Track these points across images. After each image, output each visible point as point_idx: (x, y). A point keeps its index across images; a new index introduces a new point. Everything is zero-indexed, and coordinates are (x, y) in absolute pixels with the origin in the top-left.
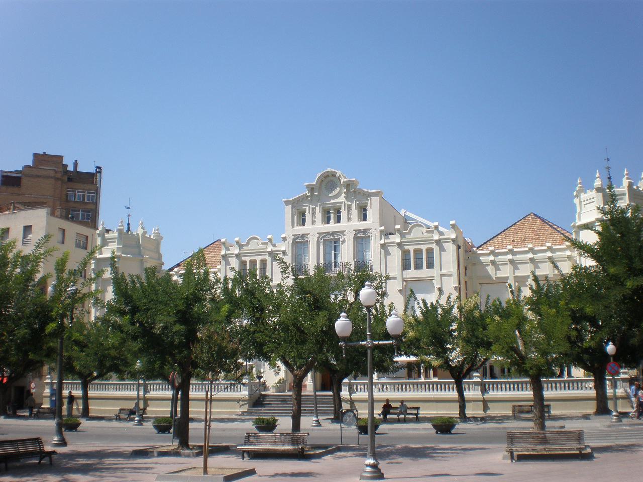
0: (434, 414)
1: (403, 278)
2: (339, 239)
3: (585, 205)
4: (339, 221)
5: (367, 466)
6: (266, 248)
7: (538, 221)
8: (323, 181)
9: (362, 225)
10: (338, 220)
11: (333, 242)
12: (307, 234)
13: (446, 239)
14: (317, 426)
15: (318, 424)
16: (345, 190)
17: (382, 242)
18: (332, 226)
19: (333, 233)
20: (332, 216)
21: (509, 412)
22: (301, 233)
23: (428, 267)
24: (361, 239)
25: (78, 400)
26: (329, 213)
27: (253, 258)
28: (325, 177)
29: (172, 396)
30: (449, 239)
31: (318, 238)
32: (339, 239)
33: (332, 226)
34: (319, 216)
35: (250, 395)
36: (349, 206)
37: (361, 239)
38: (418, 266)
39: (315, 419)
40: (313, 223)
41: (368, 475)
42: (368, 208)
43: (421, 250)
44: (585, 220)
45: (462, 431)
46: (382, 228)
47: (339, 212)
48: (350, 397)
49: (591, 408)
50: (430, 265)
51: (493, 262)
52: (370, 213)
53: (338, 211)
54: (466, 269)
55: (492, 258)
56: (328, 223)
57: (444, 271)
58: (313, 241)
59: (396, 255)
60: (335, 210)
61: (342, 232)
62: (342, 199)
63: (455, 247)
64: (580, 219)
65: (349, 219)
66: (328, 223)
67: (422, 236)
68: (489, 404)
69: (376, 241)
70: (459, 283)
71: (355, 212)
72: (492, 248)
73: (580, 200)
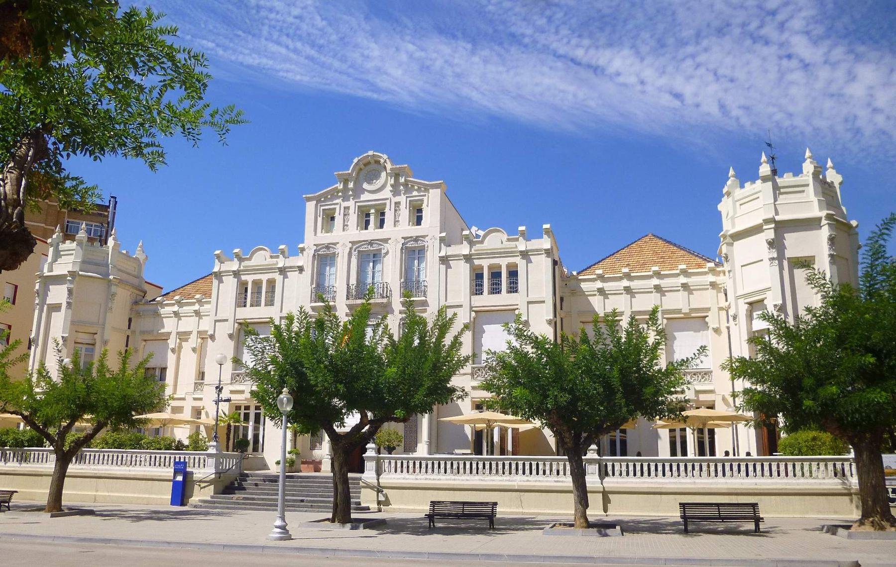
0: (549, 514)
1: (471, 307)
4: (381, 226)
6: (277, 263)
7: (660, 242)
8: (361, 169)
9: (416, 231)
10: (381, 224)
11: (372, 256)
12: (335, 244)
13: (537, 250)
14: (281, 539)
15: (286, 535)
16: (392, 182)
17: (443, 254)
18: (372, 233)
19: (371, 243)
20: (372, 218)
21: (675, 515)
22: (326, 242)
23: (509, 292)
24: (413, 252)
26: (368, 215)
28: (365, 165)
29: (573, 518)
30: (540, 250)
31: (351, 249)
33: (372, 233)
34: (353, 218)
35: (218, 473)
36: (397, 204)
37: (413, 252)
39: (279, 522)
40: (345, 227)
42: (424, 206)
46: (444, 234)
47: (383, 214)
48: (378, 480)
49: (163, 496)
50: (513, 288)
51: (601, 291)
52: (426, 214)
54: (562, 299)
55: (599, 284)
56: (366, 228)
57: (533, 297)
58: (342, 252)
59: (461, 273)
60: (377, 211)
61: (386, 241)
62: (387, 193)
63: (549, 261)
64: (51, 270)
65: (396, 222)
67: (500, 246)
68: (610, 496)
69: (433, 254)
70: (555, 316)
71: (405, 213)
72: (599, 272)
73: (733, 198)
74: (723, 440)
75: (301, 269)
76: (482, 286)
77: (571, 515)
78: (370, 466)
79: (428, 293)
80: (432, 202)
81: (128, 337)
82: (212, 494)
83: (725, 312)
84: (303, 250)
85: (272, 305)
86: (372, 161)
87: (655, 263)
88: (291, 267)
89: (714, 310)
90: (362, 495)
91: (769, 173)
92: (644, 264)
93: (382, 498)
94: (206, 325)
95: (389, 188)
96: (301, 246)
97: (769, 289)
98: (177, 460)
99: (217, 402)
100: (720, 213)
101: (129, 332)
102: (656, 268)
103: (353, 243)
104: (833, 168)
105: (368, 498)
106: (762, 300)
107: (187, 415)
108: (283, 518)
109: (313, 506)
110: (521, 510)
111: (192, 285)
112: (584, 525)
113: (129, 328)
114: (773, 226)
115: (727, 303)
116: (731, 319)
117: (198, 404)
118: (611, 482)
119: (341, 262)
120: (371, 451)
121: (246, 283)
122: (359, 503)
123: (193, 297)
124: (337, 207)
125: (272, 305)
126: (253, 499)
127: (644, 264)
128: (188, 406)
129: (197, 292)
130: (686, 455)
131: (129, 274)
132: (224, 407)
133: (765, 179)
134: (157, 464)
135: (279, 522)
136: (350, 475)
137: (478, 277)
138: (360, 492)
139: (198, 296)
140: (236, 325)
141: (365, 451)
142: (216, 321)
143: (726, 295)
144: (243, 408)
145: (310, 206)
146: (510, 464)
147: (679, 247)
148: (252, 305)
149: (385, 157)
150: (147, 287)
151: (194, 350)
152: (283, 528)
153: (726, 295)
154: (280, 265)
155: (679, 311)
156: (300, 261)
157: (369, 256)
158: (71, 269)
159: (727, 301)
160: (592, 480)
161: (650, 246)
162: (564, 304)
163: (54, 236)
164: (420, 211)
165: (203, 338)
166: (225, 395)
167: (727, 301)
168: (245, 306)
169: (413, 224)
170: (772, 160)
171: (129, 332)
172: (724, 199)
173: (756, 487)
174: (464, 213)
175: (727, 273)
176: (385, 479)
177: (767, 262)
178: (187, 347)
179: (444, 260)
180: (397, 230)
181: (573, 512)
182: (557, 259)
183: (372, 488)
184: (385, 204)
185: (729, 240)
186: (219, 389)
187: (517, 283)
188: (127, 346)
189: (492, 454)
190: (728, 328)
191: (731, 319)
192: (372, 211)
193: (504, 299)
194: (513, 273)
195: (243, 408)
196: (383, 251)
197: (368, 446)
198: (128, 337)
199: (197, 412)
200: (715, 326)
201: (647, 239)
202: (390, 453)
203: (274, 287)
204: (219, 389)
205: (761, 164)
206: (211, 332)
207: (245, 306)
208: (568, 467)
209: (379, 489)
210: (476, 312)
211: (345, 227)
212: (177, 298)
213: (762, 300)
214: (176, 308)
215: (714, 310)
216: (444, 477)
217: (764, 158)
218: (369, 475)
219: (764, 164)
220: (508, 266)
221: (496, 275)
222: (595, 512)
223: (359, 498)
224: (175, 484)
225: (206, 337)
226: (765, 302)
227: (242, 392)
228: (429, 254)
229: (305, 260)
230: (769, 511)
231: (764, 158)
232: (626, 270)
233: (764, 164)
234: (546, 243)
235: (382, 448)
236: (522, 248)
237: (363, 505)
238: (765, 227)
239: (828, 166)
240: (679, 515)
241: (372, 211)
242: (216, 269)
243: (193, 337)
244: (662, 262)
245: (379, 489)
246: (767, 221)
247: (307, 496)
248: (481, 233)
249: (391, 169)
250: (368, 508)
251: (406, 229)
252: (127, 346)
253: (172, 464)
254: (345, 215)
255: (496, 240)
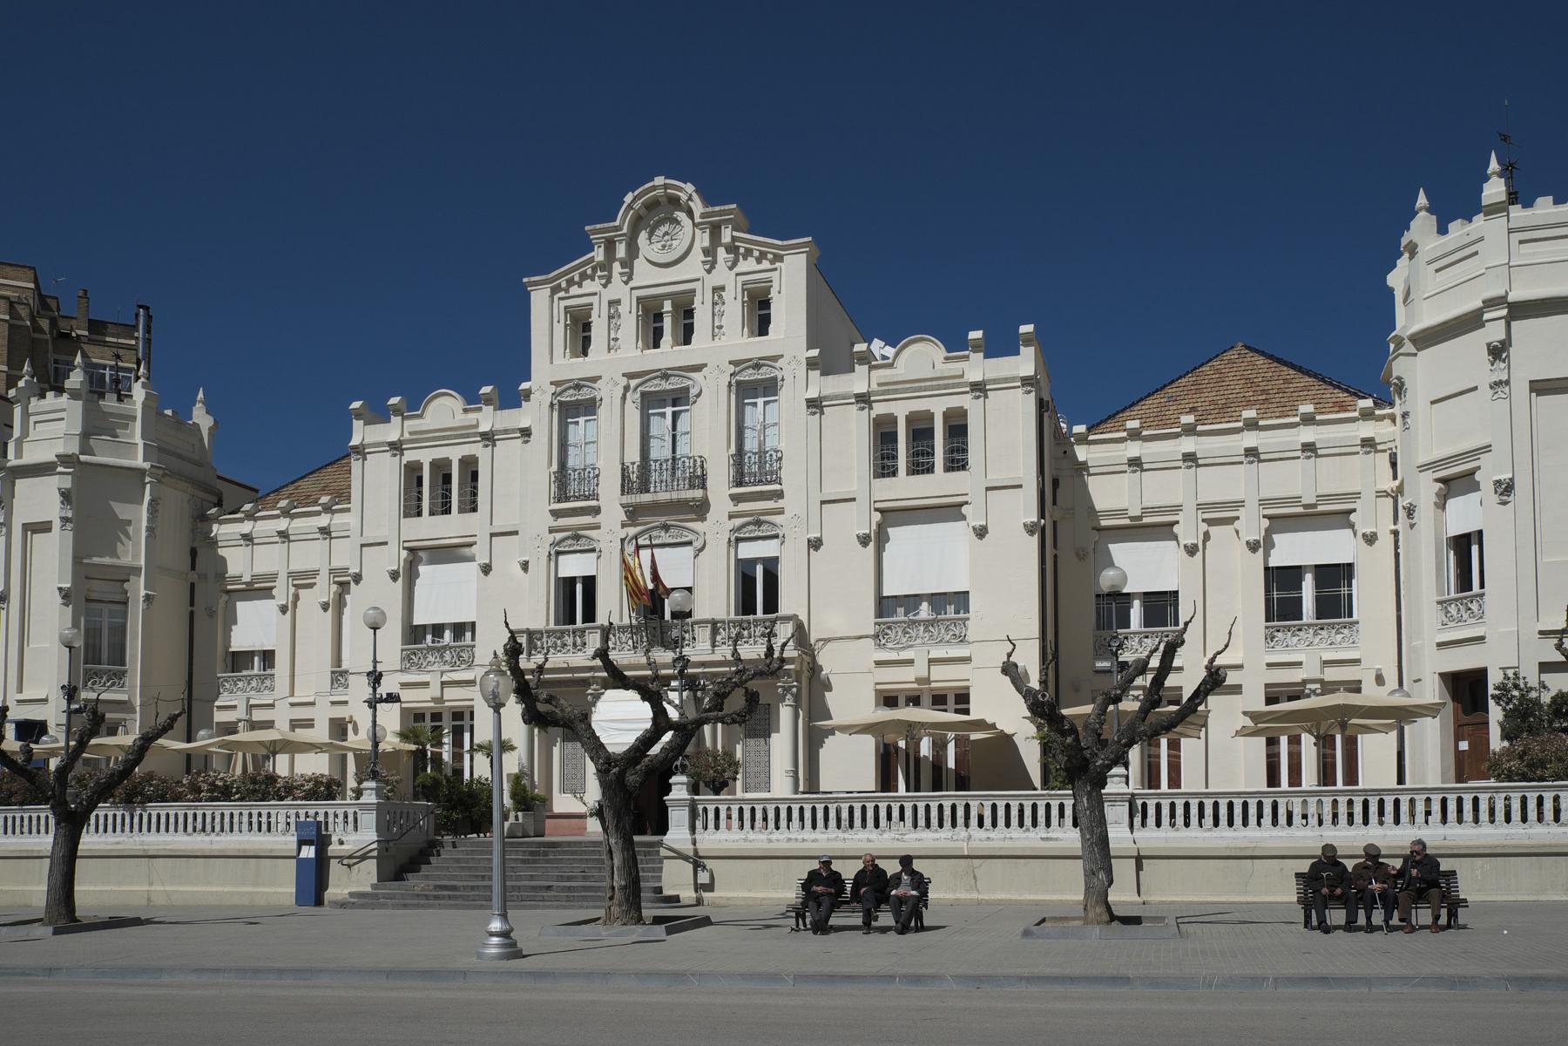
2: (687, 389)
3: (1521, 242)
4: (687, 340)
5: (492, 934)
6: (477, 426)
10: (686, 335)
12: (595, 379)
15: (513, 951)
16: (706, 243)
18: (669, 354)
20: (667, 323)
23: (948, 469)
25: (1394, 734)
26: (659, 317)
27: (440, 453)
31: (627, 388)
32: (687, 389)
36: (718, 290)
38: (920, 466)
39: (496, 925)
41: (494, 951)
42: (773, 294)
43: (929, 416)
44: (34, 454)
45: (723, 902)
46: (815, 352)
50: (957, 462)
52: (777, 311)
53: (686, 314)
54: (1056, 483)
56: (656, 345)
57: (995, 478)
58: (610, 392)
59: (851, 434)
61: (698, 368)
62: (694, 266)
64: (19, 454)
66: (656, 345)
70: (1042, 515)
71: (734, 308)
72: (1133, 424)
74: (1376, 755)
75: (526, 433)
76: (895, 457)
77: (1077, 903)
78: (678, 818)
79: (709, 484)
80: (791, 278)
81: (192, 585)
82: (375, 881)
83: (1390, 501)
84: (527, 395)
85: (474, 510)
86: (663, 200)
87: (1249, 404)
88: (506, 431)
89: (1368, 496)
90: (664, 875)
91: (1503, 197)
92: (1225, 406)
93: (704, 878)
94: (344, 555)
95: (697, 256)
96: (524, 386)
97: (1487, 449)
98: (302, 819)
99: (373, 703)
100: (1392, 290)
101: (193, 577)
102: (1250, 414)
103: (630, 376)
104: (1430, 210)
105: (676, 879)
106: (1472, 473)
107: (320, 733)
108: (504, 916)
109: (571, 897)
110: (975, 896)
111: (312, 478)
112: (1106, 917)
113: (193, 568)
114: (1504, 312)
115: (1397, 483)
116: (1402, 514)
117: (339, 712)
118: (709, 840)
119: (607, 413)
120: (679, 789)
121: (892, 420)
122: (659, 890)
123: (315, 503)
124: (594, 300)
125: (474, 510)
126: (454, 888)
127: (1225, 406)
128: (323, 716)
129: (324, 490)
130: (1179, 787)
131: (180, 457)
132: (390, 718)
133: (75, 395)
134: (218, 828)
135: (496, 925)
136: (636, 838)
137: (884, 434)
138: (661, 869)
139: (324, 499)
140: (404, 554)
141: (667, 789)
142: (492, 535)
143: (1394, 465)
144: (428, 718)
145: (540, 299)
146: (1412, 802)
147: (1300, 369)
148: (432, 513)
149: (690, 188)
150: (220, 485)
151: (325, 607)
152: (505, 934)
153: (1394, 465)
154: (485, 427)
155: (1296, 500)
156: (522, 417)
157: (665, 397)
158: (61, 451)
159: (1395, 478)
160: (1119, 834)
161: (1240, 365)
162: (1059, 491)
163: (21, 384)
164: (765, 304)
165: (341, 584)
166: (387, 686)
167: (1395, 478)
168: (419, 514)
169: (752, 334)
170: (1508, 171)
171: (193, 577)
172: (1403, 262)
173: (1446, 843)
174: (859, 309)
175: (1399, 419)
176: (709, 840)
177: (1485, 392)
178: (311, 600)
179: (815, 405)
180: (721, 342)
181: (1081, 897)
182: (1046, 398)
183: (686, 858)
184: (694, 291)
185: (1408, 347)
186: (376, 678)
187: (965, 451)
188: (192, 604)
189: (918, 790)
190: (1396, 533)
191: (1402, 514)
192: (668, 306)
193: (937, 485)
194: (957, 429)
195: (428, 718)
196: (693, 392)
197: (673, 780)
198: (192, 585)
199: (340, 728)
200: (1368, 531)
201: (1232, 355)
202: (717, 793)
203: (475, 476)
204: (376, 678)
205: (1487, 178)
206: (354, 570)
207: (419, 514)
208: (52, 822)
209: (697, 862)
210: (882, 511)
211: (716, 331)
212: (283, 503)
213: (1472, 473)
214: (324, 520)
215: (1368, 496)
216: (825, 836)
217: (1494, 165)
218: (678, 834)
219: (1495, 179)
220: (947, 415)
221: (921, 431)
222: (1121, 895)
223: (659, 879)
224: (302, 864)
225: (345, 583)
226: (1478, 476)
227: (426, 684)
228: (784, 393)
229: (535, 414)
230: (1472, 884)
231: (1494, 165)
232: (1188, 419)
233: (1495, 179)
234: (1025, 363)
235: (702, 785)
236: (974, 375)
237: (667, 892)
238: (1486, 316)
239: (1418, 205)
240: (1295, 899)
241: (668, 306)
242: (355, 441)
243: (322, 580)
244: (1265, 402)
245: (697, 862)
246: (1491, 303)
247: (561, 879)
248: (890, 351)
249: (703, 216)
250: (676, 899)
251: (738, 342)
252: (192, 604)
253: (293, 827)
254: (610, 317)
255: (922, 357)
